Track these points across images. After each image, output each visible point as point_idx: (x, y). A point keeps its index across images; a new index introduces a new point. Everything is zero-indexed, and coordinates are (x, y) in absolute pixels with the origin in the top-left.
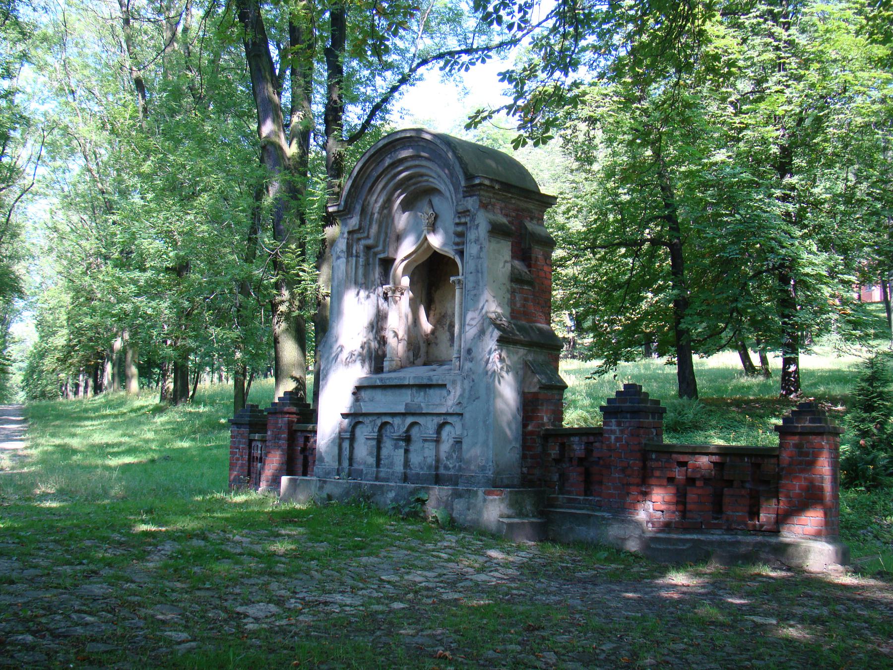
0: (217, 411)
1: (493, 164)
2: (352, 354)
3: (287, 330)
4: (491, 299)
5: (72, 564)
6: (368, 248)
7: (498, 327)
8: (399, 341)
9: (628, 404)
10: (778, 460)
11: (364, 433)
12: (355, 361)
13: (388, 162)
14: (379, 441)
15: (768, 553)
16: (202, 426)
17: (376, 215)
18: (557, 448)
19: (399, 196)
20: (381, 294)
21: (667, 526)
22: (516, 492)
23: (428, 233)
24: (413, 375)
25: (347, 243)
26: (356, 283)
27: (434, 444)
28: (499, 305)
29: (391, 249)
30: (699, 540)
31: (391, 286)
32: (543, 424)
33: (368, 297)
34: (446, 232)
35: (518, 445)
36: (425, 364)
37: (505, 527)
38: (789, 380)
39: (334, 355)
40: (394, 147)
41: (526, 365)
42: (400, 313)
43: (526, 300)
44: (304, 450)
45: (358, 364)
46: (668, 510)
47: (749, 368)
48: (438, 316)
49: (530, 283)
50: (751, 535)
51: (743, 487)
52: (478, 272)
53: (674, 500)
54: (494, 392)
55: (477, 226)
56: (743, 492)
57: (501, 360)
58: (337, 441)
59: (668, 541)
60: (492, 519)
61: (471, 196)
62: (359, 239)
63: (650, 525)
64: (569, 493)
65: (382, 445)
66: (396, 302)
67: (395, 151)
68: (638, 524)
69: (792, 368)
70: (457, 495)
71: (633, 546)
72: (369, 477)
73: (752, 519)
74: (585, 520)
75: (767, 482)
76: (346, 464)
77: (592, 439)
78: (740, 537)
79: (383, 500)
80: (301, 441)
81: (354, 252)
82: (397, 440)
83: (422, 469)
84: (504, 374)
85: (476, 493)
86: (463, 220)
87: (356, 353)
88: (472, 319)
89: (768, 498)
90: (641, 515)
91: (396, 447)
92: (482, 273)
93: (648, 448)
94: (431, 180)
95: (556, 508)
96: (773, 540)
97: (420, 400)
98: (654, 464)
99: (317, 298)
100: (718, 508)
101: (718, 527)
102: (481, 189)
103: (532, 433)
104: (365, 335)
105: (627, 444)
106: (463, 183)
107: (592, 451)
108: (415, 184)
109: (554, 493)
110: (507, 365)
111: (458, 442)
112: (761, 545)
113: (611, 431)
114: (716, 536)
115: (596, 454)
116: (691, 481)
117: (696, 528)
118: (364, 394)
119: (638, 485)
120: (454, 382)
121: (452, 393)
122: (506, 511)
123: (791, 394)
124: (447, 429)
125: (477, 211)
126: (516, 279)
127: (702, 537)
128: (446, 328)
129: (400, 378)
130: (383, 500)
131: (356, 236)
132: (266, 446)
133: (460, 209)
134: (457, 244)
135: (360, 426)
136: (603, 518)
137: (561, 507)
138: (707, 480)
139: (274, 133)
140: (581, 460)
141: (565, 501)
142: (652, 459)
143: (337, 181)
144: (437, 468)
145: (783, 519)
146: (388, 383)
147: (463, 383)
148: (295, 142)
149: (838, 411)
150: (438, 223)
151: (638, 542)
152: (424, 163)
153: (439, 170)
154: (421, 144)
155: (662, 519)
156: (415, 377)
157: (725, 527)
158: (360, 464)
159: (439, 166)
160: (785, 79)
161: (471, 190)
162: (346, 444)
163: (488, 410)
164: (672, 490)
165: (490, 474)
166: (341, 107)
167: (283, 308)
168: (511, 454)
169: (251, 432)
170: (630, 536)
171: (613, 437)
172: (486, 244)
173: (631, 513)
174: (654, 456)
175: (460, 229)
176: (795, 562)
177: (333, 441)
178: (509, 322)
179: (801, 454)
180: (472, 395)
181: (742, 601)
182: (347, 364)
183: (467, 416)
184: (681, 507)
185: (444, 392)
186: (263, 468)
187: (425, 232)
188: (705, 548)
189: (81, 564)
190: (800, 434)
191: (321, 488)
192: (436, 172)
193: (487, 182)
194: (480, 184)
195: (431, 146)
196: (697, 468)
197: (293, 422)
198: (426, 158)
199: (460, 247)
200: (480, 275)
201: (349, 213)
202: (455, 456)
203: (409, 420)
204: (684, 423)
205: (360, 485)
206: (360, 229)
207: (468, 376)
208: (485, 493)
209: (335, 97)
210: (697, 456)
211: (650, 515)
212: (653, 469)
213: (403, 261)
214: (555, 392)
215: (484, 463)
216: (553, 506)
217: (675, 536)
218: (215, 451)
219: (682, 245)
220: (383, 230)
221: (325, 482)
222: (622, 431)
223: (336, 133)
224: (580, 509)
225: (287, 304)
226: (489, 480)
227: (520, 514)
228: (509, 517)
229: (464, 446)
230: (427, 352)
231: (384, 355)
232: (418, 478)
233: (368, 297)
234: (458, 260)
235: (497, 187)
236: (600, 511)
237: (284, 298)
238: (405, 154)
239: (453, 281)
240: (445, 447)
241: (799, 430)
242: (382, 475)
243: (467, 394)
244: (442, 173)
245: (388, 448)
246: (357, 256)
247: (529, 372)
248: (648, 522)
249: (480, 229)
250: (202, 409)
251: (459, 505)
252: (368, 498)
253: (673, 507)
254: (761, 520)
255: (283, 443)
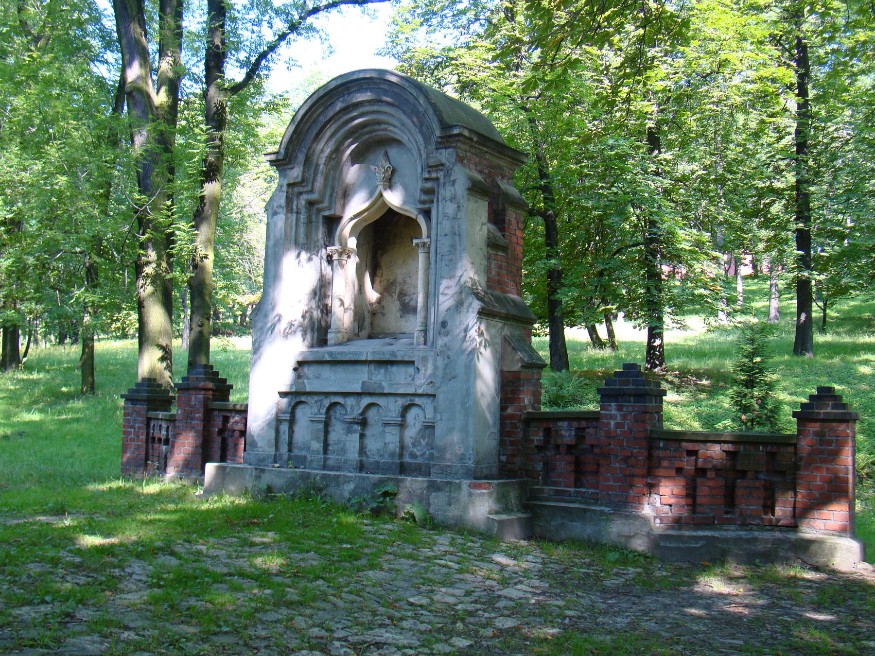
0: (53, 378)
1: (464, 115)
2: (291, 325)
3: (153, 293)
4: (469, 266)
5: (30, 603)
6: (311, 204)
7: (477, 295)
8: (346, 310)
9: (631, 387)
10: (795, 448)
11: (304, 415)
12: (295, 332)
13: (339, 106)
14: (327, 424)
15: (787, 550)
16: (43, 395)
17: (322, 166)
18: (541, 434)
19: (349, 146)
20: (325, 257)
21: (678, 522)
22: (503, 484)
23: (385, 189)
24: (370, 350)
25: (287, 197)
26: (296, 244)
27: (398, 428)
28: (476, 273)
29: (338, 206)
30: (713, 537)
31: (337, 247)
32: (525, 407)
33: (310, 259)
34: (406, 189)
35: (495, 430)
36: (370, 337)
37: (496, 524)
38: (654, 354)
39: (269, 325)
40: (348, 89)
41: (505, 340)
42: (346, 278)
43: (500, 267)
44: (221, 432)
45: (299, 336)
46: (677, 504)
47: (597, 342)
48: (385, 283)
49: (504, 249)
50: (767, 530)
51: (757, 478)
52: (455, 234)
53: (684, 493)
54: (475, 372)
55: (454, 182)
56: (757, 484)
57: (481, 334)
58: (274, 423)
59: (679, 538)
60: (480, 517)
61: (446, 148)
62: (301, 193)
63: (658, 521)
64: (555, 484)
65: (330, 429)
66: (342, 266)
67: (349, 94)
68: (645, 520)
69: (658, 342)
70: (434, 487)
71: (640, 545)
72: (315, 465)
73: (766, 513)
74: (581, 515)
75: (782, 473)
76: (284, 449)
77: (584, 424)
78: (756, 533)
79: (338, 492)
80: (219, 422)
81: (294, 207)
82: (350, 423)
83: (382, 456)
84: (482, 350)
85: (459, 487)
86: (434, 175)
87: (296, 323)
88: (448, 287)
89: (786, 490)
90: (647, 510)
91: (349, 431)
92: (459, 235)
93: (654, 436)
94: (391, 128)
95: (541, 501)
96: (791, 536)
97: (379, 378)
98: (661, 453)
99: (194, 260)
100: (730, 500)
101: (730, 522)
102: (459, 141)
103: (512, 417)
104: (306, 302)
105: (630, 430)
106: (438, 133)
107: (584, 437)
108: (368, 133)
109: (537, 484)
110: (486, 340)
111: (429, 428)
112: (779, 542)
113: (611, 415)
114: (731, 532)
115: (589, 440)
116: (701, 472)
117: (708, 523)
118: (306, 370)
119: (643, 476)
120: (424, 359)
121: (422, 371)
122: (495, 507)
123: (656, 367)
124: (413, 413)
125: (454, 165)
126: (492, 244)
127: (716, 534)
128: (396, 297)
129: (355, 353)
130: (338, 492)
131: (296, 190)
132: (175, 427)
133: (432, 162)
134: (423, 202)
135: (301, 407)
136: (602, 513)
137: (547, 500)
138: (717, 470)
139: (139, 78)
140: (570, 448)
141: (552, 493)
142: (659, 448)
143: (219, 134)
144: (401, 455)
145: (800, 514)
146: (340, 358)
147: (435, 361)
148: (163, 89)
149: (704, 385)
150: (396, 178)
151: (646, 540)
152: (384, 108)
153: (403, 117)
154: (383, 86)
155: (670, 514)
156: (374, 353)
157: (739, 523)
158: (302, 449)
159: (404, 112)
160: (659, 55)
161: (447, 140)
162: (285, 427)
163: (467, 390)
164: (681, 482)
165: (471, 464)
166: (223, 53)
167: (149, 270)
168: (489, 442)
169: (149, 410)
170: (636, 534)
171: (612, 423)
172: (464, 203)
173: (635, 508)
174: (661, 445)
175: (429, 185)
176: (821, 560)
177: (269, 424)
178: (486, 293)
179: (822, 442)
180: (449, 375)
181: (829, 617)
182: (286, 335)
183: (441, 397)
184: (690, 501)
185: (411, 370)
186: (171, 451)
187: (380, 188)
188: (720, 545)
189: (44, 602)
190: (822, 421)
191: (258, 477)
192: (399, 119)
193: (466, 133)
194: (459, 135)
195: (396, 90)
196: (708, 459)
197: (208, 399)
198: (388, 103)
199: (427, 206)
200: (457, 238)
201: (290, 162)
202: (423, 442)
203: (366, 401)
204: (563, 397)
205: (308, 476)
206: (303, 182)
207: (445, 353)
208: (470, 486)
209: (217, 42)
210: (709, 444)
211: (656, 510)
212: (660, 459)
213: (351, 219)
214: (535, 371)
215: (462, 451)
216: (537, 499)
217: (687, 533)
218: (75, 426)
219: (556, 216)
220: (330, 183)
221: (263, 471)
222: (624, 417)
223: (219, 80)
224: (571, 502)
225: (154, 265)
226: (469, 470)
227: (506, 510)
228: (497, 513)
229: (438, 431)
230: (372, 323)
231: (328, 327)
232: (377, 468)
233: (310, 259)
234: (421, 221)
235: (475, 139)
236: (596, 504)
237: (150, 259)
238: (360, 97)
239: (417, 245)
240: (411, 433)
241: (822, 417)
242: (331, 462)
243: (440, 373)
244: (408, 121)
245: (337, 432)
246: (298, 213)
247: (509, 349)
248: (655, 518)
249: (457, 185)
250: (35, 376)
251: (437, 500)
252: (320, 490)
253: (683, 502)
254: (776, 514)
255: (198, 424)
